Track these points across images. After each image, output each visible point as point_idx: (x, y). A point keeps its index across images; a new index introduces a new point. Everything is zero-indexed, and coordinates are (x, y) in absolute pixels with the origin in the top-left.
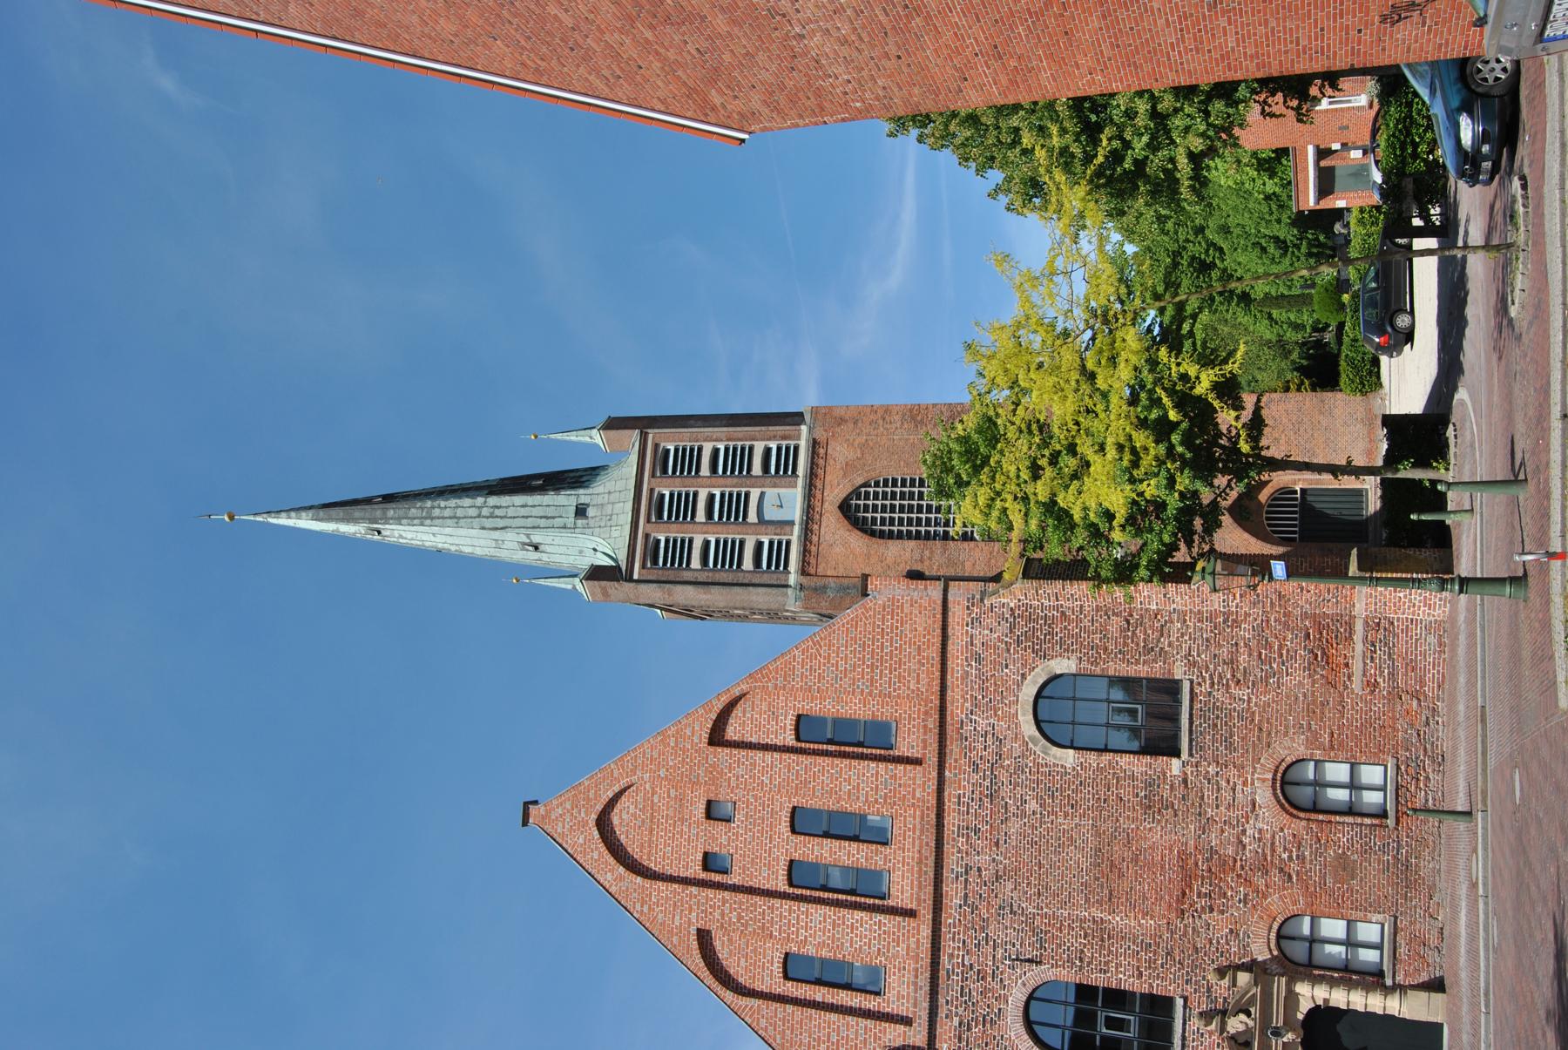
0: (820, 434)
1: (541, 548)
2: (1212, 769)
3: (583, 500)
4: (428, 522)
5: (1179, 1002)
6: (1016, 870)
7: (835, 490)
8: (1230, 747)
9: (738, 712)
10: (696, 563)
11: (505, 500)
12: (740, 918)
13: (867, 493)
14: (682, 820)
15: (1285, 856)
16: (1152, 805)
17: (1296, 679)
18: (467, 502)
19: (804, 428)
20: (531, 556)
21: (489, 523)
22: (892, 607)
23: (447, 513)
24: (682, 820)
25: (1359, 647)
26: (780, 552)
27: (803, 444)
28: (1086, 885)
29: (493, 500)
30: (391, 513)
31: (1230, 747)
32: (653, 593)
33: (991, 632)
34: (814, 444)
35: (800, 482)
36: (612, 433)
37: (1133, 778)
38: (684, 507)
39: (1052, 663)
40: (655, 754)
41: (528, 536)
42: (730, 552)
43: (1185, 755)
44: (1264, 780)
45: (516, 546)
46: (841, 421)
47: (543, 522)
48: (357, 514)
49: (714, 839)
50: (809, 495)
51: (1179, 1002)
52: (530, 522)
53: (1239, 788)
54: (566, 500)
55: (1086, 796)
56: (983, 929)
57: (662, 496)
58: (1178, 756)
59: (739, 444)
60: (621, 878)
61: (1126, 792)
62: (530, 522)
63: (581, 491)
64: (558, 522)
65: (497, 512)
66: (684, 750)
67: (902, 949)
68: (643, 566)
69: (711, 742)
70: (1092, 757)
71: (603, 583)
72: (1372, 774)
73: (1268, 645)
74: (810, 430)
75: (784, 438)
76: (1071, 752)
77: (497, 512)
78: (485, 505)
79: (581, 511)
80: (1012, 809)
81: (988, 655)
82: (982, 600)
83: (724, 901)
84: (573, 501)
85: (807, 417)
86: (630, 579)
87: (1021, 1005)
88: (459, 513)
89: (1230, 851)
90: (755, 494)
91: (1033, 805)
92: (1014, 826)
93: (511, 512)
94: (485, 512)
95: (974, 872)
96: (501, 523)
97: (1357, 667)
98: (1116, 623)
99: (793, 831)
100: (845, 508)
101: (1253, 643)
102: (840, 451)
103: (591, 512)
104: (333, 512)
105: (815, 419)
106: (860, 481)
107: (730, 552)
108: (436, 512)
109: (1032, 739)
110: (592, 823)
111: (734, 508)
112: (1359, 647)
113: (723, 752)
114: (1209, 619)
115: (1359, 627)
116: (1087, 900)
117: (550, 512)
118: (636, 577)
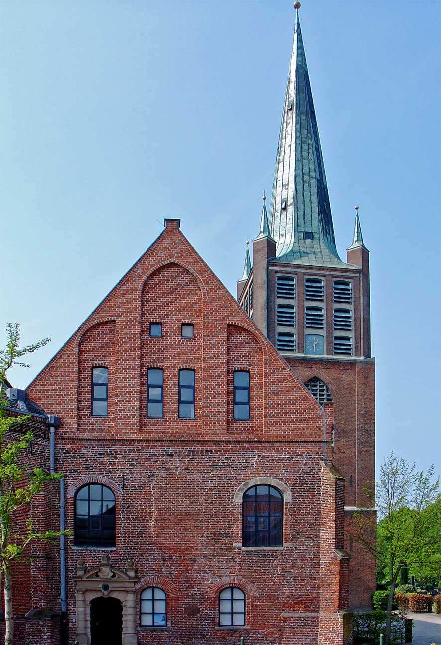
0: (358, 367)
1: (284, 212)
2: (237, 560)
3: (317, 236)
4: (299, 142)
5: (114, 549)
6: (173, 478)
7: (323, 374)
8: (249, 567)
9: (244, 334)
10: (280, 301)
11: (314, 190)
12: (126, 343)
13: (323, 390)
14: (180, 311)
15: (196, 589)
16: (216, 536)
17: (286, 591)
18: (312, 167)
19: (362, 358)
20: (291, 209)
21: (300, 179)
22: (316, 418)
23: (305, 154)
24: (180, 311)
25: (304, 614)
26: (289, 347)
27: (353, 358)
28: (170, 509)
29: (314, 182)
30: (304, 118)
31: (249, 567)
32: (261, 277)
33: (304, 464)
34: (352, 364)
35: (330, 357)
36: (360, 254)
37: (230, 528)
38: (314, 293)
39: (289, 492)
40: (219, 295)
41: (291, 204)
42: (287, 320)
43: (243, 548)
44: (234, 580)
45: (284, 196)
46: (366, 378)
47: (301, 212)
48: (302, 95)
49: (171, 328)
50: (321, 361)
51: (114, 549)
52: (301, 205)
53: (230, 571)
54: (315, 226)
55: (217, 508)
56: (138, 463)
57: (320, 282)
58: (243, 546)
59: (352, 324)
60: (140, 278)
61: (222, 525)
62: (301, 205)
63: (322, 235)
64: (301, 222)
65: (306, 185)
66: (223, 311)
67: (120, 425)
68: (277, 272)
69: (229, 326)
70: (240, 510)
71: (265, 249)
72: (239, 620)
73: (303, 580)
74: (360, 362)
75: (356, 348)
76: (242, 501)
77: (306, 185)
78: (311, 177)
79: (309, 236)
80: (207, 475)
81: (291, 463)
82: (322, 460)
83: (134, 335)
84: (315, 231)
85: (368, 360)
86: (269, 264)
87: (99, 481)
88: (305, 162)
89: (196, 568)
90: (323, 333)
91: (210, 485)
92: (197, 476)
93: (307, 193)
94: (307, 178)
95: (169, 459)
96: (300, 188)
97: (294, 614)
98: (312, 519)
99: (180, 370)
100: (315, 379)
101: (304, 575)
102: (348, 377)
103: (308, 241)
104: (303, 79)
105: (367, 364)
106: (331, 387)
107: (287, 320)
108: (305, 147)
109: (247, 484)
110: (172, 260)
111: (314, 322)
112: (304, 614)
113: (224, 333)
114: (316, 557)
115: (313, 614)
116: (161, 510)
117: (308, 218)
118: (270, 268)
